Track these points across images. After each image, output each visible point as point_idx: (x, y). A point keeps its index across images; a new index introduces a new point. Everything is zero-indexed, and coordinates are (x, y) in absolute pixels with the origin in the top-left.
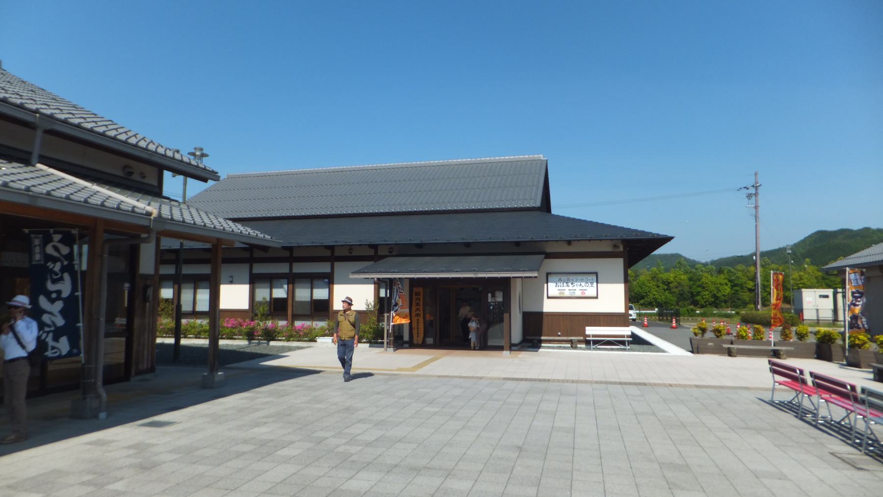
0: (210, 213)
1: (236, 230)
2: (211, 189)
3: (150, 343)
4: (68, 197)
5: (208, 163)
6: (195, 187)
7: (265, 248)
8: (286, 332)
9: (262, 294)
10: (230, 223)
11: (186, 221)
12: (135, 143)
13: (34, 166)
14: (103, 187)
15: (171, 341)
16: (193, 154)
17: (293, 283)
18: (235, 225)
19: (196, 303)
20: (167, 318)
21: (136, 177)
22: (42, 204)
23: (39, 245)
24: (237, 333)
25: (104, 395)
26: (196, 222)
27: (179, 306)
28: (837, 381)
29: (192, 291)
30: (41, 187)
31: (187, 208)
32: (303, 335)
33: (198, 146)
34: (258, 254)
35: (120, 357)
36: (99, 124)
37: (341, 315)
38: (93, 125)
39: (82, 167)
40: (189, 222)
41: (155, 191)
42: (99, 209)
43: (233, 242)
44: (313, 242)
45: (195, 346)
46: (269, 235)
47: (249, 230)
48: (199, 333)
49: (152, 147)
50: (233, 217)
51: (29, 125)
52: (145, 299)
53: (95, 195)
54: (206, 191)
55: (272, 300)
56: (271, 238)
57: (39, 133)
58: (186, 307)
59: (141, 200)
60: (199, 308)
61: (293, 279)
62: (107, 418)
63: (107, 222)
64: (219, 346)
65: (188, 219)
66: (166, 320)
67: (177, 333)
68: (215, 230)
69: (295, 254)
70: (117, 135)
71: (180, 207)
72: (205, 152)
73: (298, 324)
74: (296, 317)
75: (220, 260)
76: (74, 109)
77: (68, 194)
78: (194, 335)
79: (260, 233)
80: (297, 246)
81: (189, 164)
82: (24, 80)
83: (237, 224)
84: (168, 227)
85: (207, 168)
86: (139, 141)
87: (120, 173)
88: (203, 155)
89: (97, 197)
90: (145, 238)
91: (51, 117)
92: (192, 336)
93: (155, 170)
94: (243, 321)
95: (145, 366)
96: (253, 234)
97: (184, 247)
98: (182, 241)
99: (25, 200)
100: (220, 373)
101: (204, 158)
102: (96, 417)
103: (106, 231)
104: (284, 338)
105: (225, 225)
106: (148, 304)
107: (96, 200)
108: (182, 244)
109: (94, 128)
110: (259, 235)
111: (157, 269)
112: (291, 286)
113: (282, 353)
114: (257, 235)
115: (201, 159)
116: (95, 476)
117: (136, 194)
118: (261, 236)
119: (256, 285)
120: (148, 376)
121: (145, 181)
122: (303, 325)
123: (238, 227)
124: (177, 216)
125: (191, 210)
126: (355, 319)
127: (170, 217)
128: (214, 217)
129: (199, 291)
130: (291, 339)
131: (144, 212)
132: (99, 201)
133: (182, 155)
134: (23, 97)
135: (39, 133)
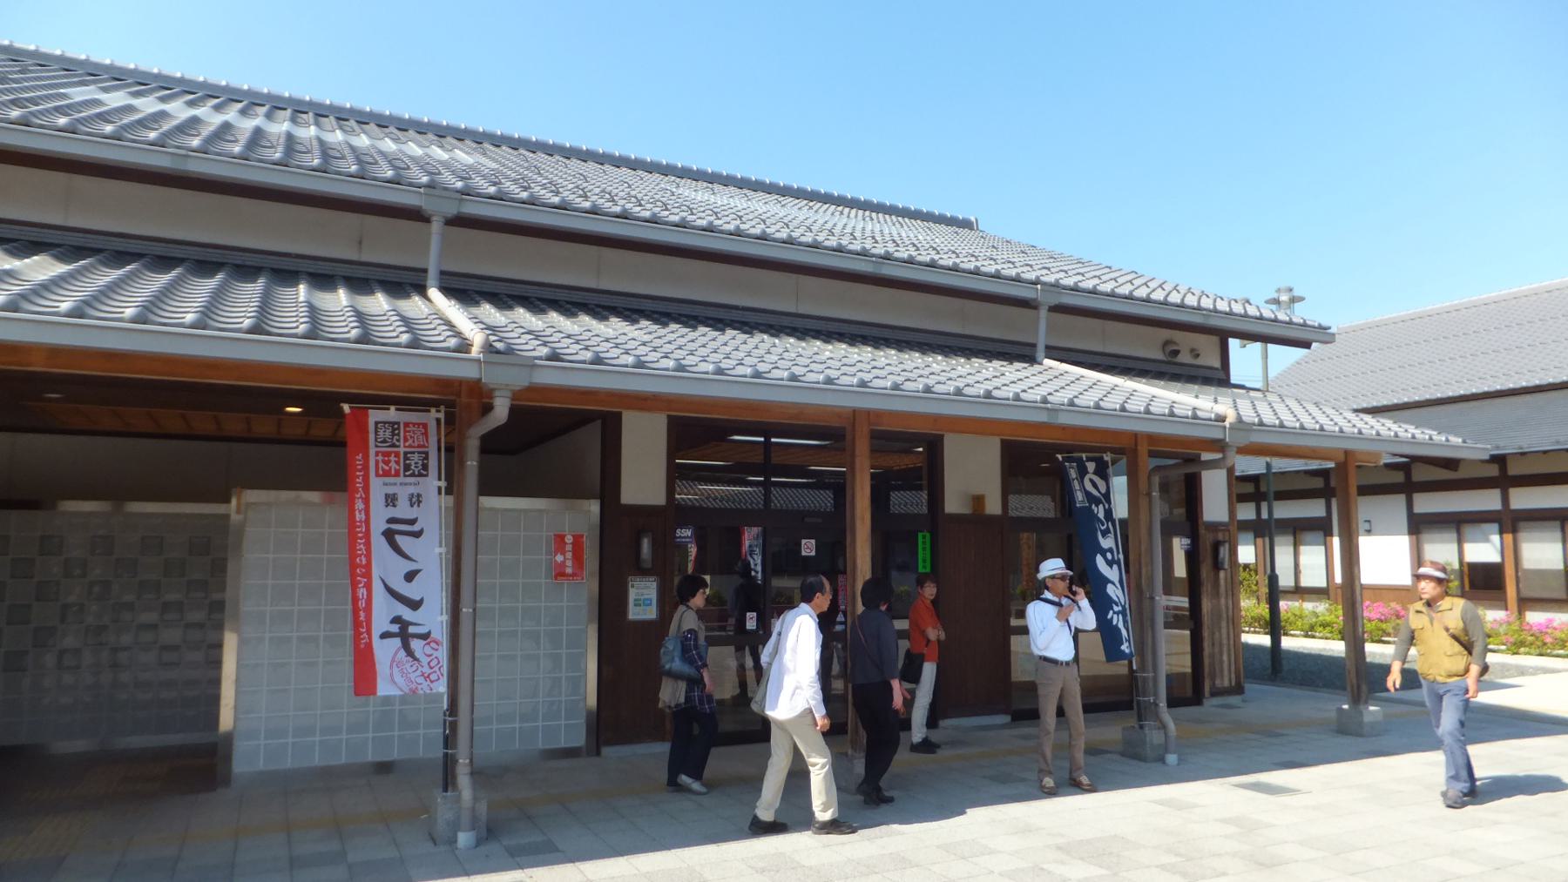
0: (1287, 396)
1: (1383, 431)
2: (1306, 360)
3: (1232, 642)
4: (1017, 398)
5: (1301, 313)
6: (1282, 357)
7: (1450, 464)
8: (1506, 634)
9: (1442, 551)
10: (1368, 418)
11: (1286, 423)
12: (1179, 301)
13: (1041, 364)
14: (1184, 391)
15: (1265, 640)
16: (1276, 302)
17: (1514, 531)
18: (1378, 421)
19: (1300, 572)
20: (1249, 598)
21: (1184, 358)
22: (1064, 419)
23: (1077, 478)
24: (1391, 631)
25: (1171, 726)
26: (1264, 420)
27: (1273, 579)
28: (577, 232)
29: (1291, 549)
30: (1058, 394)
31: (1280, 400)
32: (1551, 644)
33: (1284, 285)
34: (1421, 474)
35: (1185, 664)
36: (1121, 280)
37: (1418, 612)
38: (1096, 281)
39: (736, 308)
40: (1292, 425)
41: (1219, 378)
42: (920, 398)
43: (1378, 455)
44: (1558, 442)
45: (1306, 651)
46: (1456, 435)
47: (1412, 429)
48: (1312, 628)
49: (1207, 303)
50: (1370, 406)
51: (417, 215)
52: (1217, 566)
53: (1062, 390)
54: (1298, 363)
55: (1466, 569)
56: (1464, 442)
57: (1043, 313)
58: (1285, 580)
59: (1200, 396)
60: (1306, 582)
61: (1511, 523)
62: (1178, 764)
63: (1152, 438)
64: (1367, 654)
65: (1249, 416)
66: (1247, 601)
67: (1275, 626)
68: (1415, 440)
69: (1513, 470)
70: (1151, 293)
71: (1267, 400)
72: (1296, 293)
73: (1535, 617)
74: (1525, 603)
75: (1353, 490)
76: (1081, 265)
77: (1071, 396)
78: (1302, 630)
79: (1435, 433)
80: (1516, 453)
81: (1276, 320)
82: (1008, 239)
83: (1382, 420)
84: (1257, 438)
85: (1308, 322)
86: (1184, 296)
87: (1159, 355)
88: (1293, 300)
89: (1136, 400)
90: (1219, 459)
91: (1056, 285)
92: (1298, 632)
93: (1215, 339)
94: (1403, 609)
95: (1225, 681)
96: (1422, 436)
97: (1274, 471)
98: (1268, 459)
99: (1042, 417)
100: (1372, 708)
101: (1296, 304)
102: (1162, 760)
103: (1153, 454)
104: (1503, 647)
105: (1360, 425)
106: (1222, 574)
107: (1135, 405)
108: (1268, 466)
109: (1003, 271)
110: (1434, 437)
111: (1232, 512)
112: (1509, 537)
113: (1502, 678)
114: (1431, 439)
115: (1290, 308)
116: (1179, 859)
117: (1190, 386)
118: (1440, 438)
119: (1425, 536)
120: (1234, 700)
121: (1199, 362)
122: (1550, 621)
123: (1387, 425)
124: (1248, 415)
125: (1288, 403)
126: (1464, 623)
127: (1256, 420)
128: (1333, 412)
129: (1303, 549)
130: (1522, 650)
131: (1213, 416)
132: (1141, 406)
133: (1258, 307)
134: (1017, 265)
135: (1043, 313)
